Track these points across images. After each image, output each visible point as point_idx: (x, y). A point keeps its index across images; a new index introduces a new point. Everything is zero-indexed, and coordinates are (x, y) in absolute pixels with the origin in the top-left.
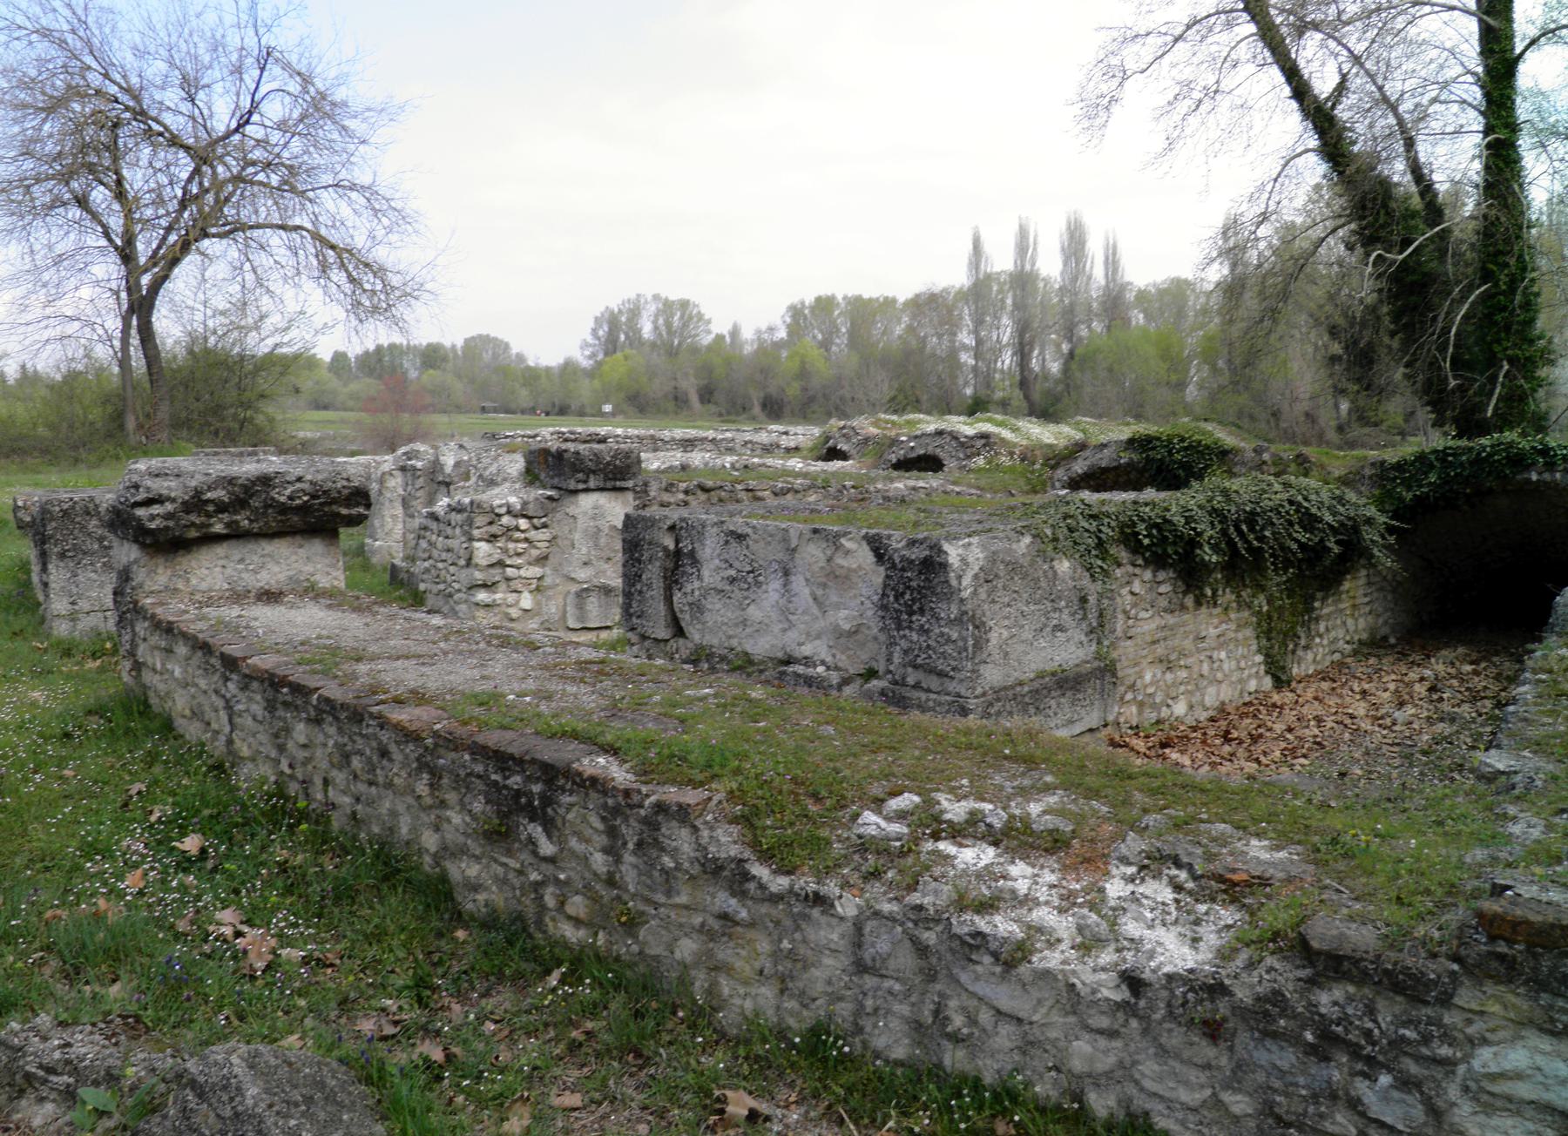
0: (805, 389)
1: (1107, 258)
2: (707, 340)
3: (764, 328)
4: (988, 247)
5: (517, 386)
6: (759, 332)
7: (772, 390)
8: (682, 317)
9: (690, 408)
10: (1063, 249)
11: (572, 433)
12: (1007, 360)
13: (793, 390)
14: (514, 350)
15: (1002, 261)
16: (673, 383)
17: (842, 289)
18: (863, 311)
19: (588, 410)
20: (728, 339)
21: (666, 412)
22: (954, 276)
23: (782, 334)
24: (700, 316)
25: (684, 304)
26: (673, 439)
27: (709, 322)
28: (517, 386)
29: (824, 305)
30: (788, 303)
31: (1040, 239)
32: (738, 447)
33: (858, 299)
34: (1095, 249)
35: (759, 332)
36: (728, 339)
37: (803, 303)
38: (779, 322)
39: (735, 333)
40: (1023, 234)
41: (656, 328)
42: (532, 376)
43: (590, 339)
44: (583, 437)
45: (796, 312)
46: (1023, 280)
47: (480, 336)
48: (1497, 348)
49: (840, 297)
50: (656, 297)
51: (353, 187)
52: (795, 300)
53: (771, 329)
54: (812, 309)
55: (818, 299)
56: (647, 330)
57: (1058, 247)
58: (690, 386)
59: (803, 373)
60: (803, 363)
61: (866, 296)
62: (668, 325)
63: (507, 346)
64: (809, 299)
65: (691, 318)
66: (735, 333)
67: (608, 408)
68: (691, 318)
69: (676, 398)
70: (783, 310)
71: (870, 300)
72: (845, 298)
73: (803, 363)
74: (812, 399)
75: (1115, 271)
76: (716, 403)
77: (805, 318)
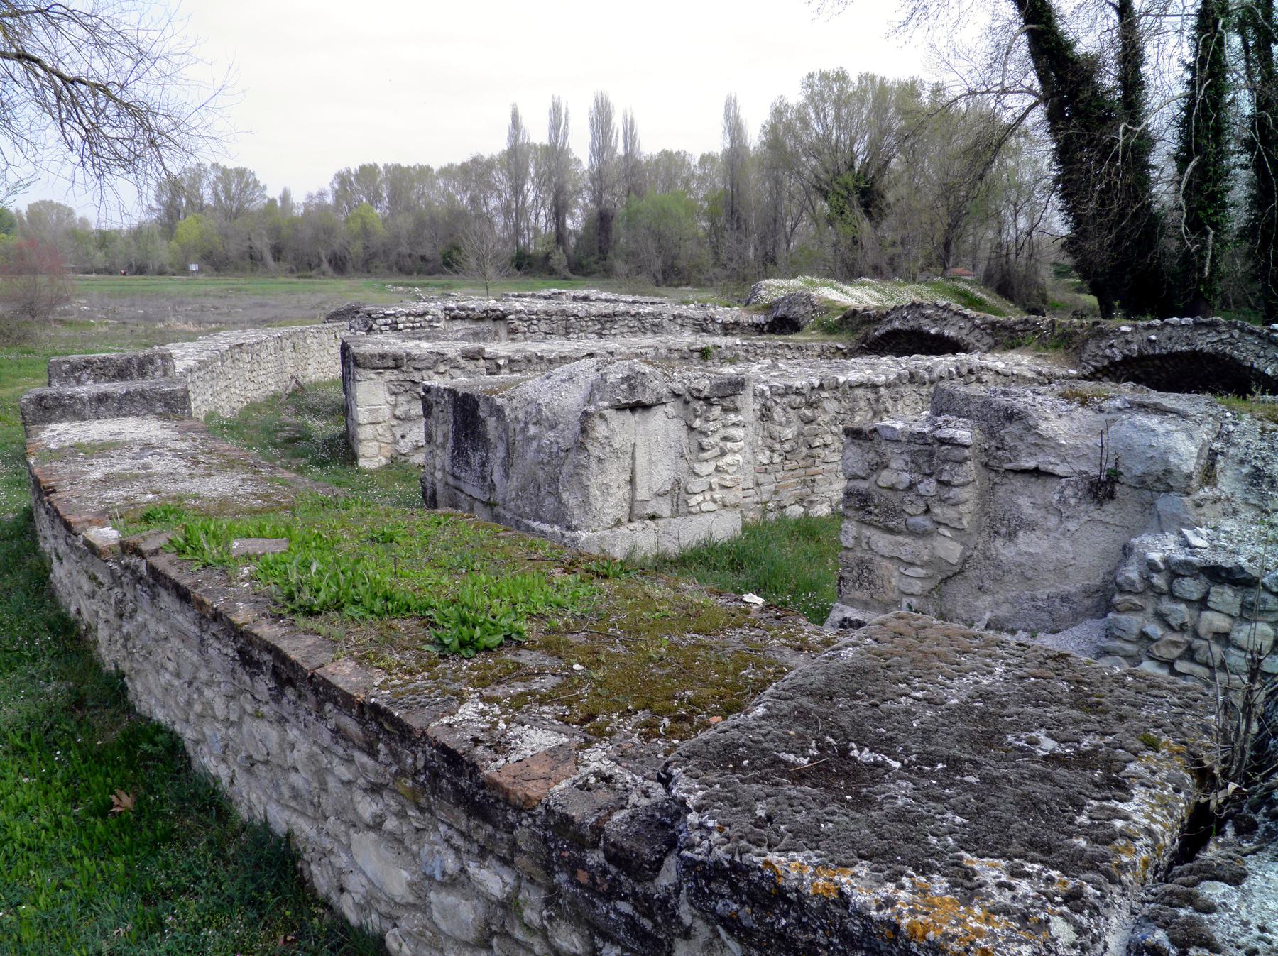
0: (366, 248)
1: (625, 133)
2: (260, 203)
3: (315, 193)
4: (525, 122)
5: (91, 248)
6: (310, 197)
7: (336, 247)
8: (239, 184)
9: (265, 266)
10: (592, 125)
11: (461, 309)
12: (542, 220)
13: (357, 248)
14: (78, 215)
15: (538, 135)
16: (248, 243)
17: (382, 159)
18: (403, 181)
19: (168, 269)
20: (279, 204)
21: (243, 270)
22: (494, 145)
23: (329, 200)
24: (256, 183)
25: (241, 173)
26: (589, 315)
27: (265, 188)
28: (91, 248)
29: (367, 172)
30: (336, 171)
31: (570, 116)
32: (665, 322)
33: (397, 168)
34: (617, 123)
35: (310, 197)
36: (279, 204)
37: (349, 171)
38: (328, 188)
39: (285, 197)
40: (556, 111)
41: (216, 194)
42: (104, 239)
43: (154, 205)
44: (478, 314)
45: (343, 179)
46: (555, 154)
47: (43, 202)
48: (1202, 214)
49: (381, 166)
50: (215, 166)
51: (1010, 47)
52: (341, 168)
53: (321, 194)
54: (357, 176)
55: (363, 168)
56: (207, 196)
57: (588, 122)
58: (263, 245)
59: (366, 232)
60: (364, 224)
61: (404, 165)
62: (227, 191)
63: (71, 212)
64: (354, 167)
65: (247, 185)
66: (285, 197)
67: (194, 267)
68: (247, 185)
69: (251, 257)
70: (331, 178)
71: (409, 168)
72: (386, 166)
73: (364, 224)
74: (373, 256)
75: (633, 143)
76: (285, 261)
77: (351, 183)
